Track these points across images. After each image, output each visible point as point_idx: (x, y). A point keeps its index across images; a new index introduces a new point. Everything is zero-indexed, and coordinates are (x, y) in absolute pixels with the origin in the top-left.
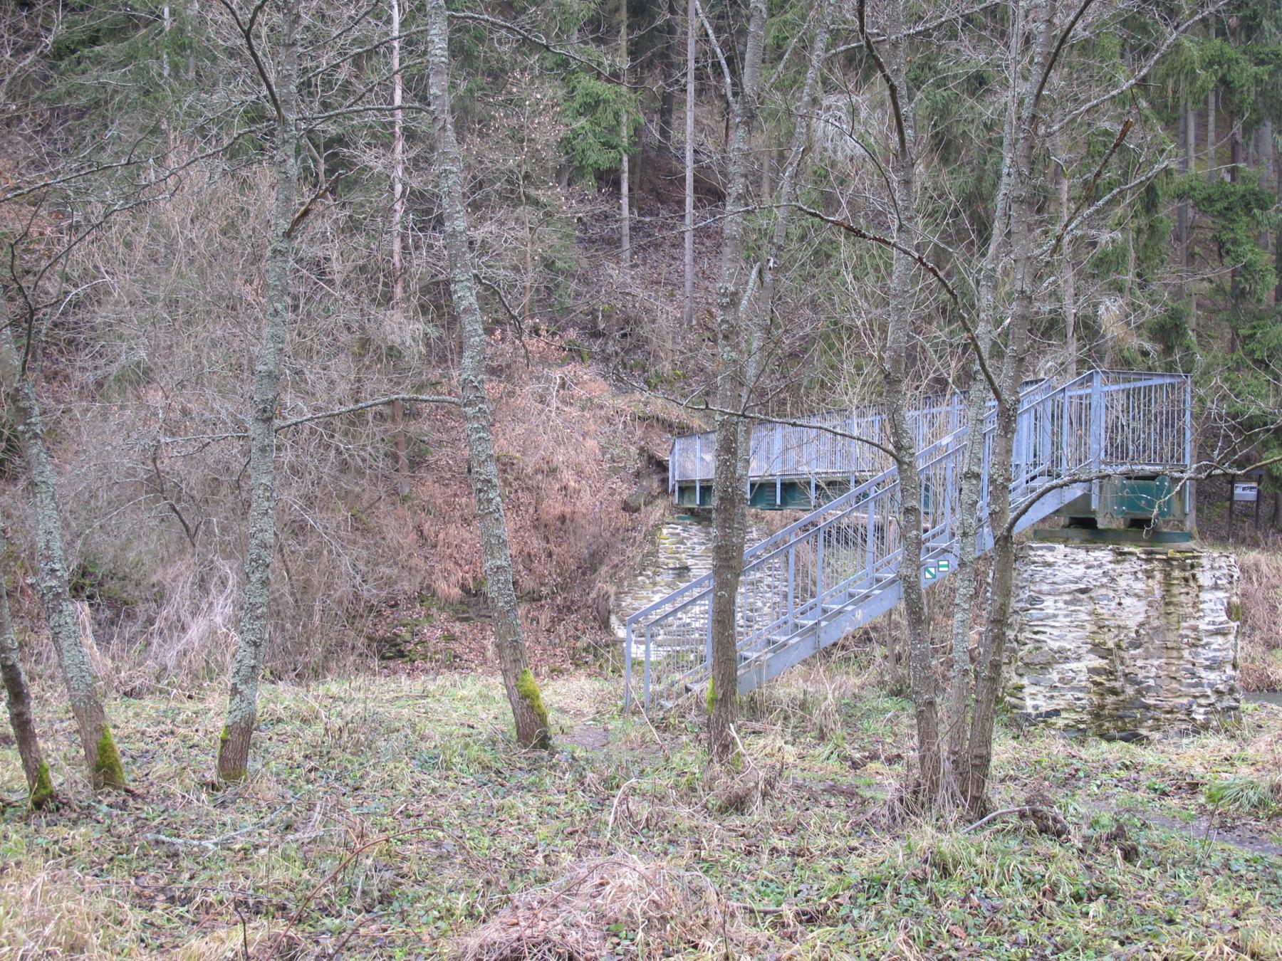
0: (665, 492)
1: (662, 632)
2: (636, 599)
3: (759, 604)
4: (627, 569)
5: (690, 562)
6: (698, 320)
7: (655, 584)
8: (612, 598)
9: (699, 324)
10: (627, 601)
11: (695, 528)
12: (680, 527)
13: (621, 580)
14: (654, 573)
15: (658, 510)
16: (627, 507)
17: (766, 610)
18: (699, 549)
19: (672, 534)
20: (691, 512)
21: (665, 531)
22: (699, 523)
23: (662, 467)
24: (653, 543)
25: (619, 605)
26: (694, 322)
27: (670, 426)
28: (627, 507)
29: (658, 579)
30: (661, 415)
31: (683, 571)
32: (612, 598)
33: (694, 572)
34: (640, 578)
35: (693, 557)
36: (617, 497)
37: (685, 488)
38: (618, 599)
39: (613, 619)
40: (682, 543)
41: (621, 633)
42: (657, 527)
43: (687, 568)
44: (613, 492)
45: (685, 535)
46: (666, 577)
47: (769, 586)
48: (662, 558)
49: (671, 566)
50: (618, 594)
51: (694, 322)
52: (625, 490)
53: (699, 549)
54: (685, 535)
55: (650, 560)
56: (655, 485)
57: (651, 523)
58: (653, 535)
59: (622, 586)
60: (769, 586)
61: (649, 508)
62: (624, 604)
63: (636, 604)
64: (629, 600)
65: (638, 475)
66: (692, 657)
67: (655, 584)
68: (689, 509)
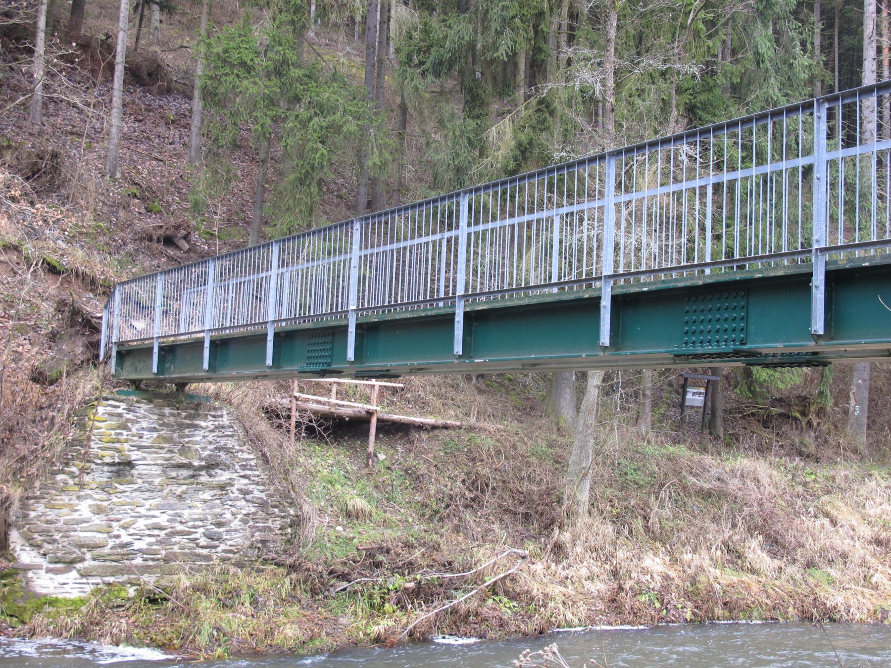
0: (93, 360)
1: (88, 556)
2: (53, 507)
3: (228, 516)
4: (40, 462)
5: (134, 455)
6: (123, 173)
7: (82, 486)
8: (16, 505)
9: (124, 177)
10: (38, 510)
11: (143, 408)
12: (123, 405)
13: (31, 479)
14: (83, 470)
15: (88, 383)
16: (38, 377)
17: (236, 524)
18: (149, 438)
19: (111, 415)
20: (136, 384)
21: (101, 410)
22: (150, 401)
23: (91, 326)
24: (82, 426)
25: (25, 516)
26: (118, 175)
27: (93, 282)
28: (38, 377)
29: (87, 478)
30: (82, 269)
31: (123, 468)
32: (16, 505)
33: (140, 469)
34: (60, 477)
35: (140, 448)
36: (24, 364)
37: (127, 353)
38: (24, 506)
39: (14, 536)
40: (125, 428)
41: (26, 556)
42: (89, 404)
43: (130, 464)
44: (17, 357)
45: (130, 416)
46: (100, 476)
47: (241, 491)
48: (95, 448)
49: (108, 460)
50: (24, 500)
51: (118, 175)
52: (34, 355)
53: (149, 438)
54: (130, 416)
55: (77, 451)
56: (79, 350)
57: (79, 398)
58: (82, 415)
59: (32, 487)
60: (241, 491)
61: (72, 381)
62: (32, 514)
63: (52, 515)
64: (41, 508)
65: (53, 337)
66: (131, 592)
67: (82, 486)
68: (133, 382)
